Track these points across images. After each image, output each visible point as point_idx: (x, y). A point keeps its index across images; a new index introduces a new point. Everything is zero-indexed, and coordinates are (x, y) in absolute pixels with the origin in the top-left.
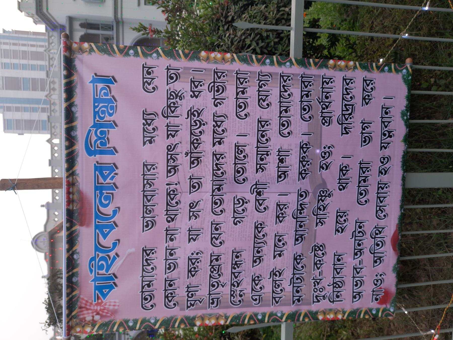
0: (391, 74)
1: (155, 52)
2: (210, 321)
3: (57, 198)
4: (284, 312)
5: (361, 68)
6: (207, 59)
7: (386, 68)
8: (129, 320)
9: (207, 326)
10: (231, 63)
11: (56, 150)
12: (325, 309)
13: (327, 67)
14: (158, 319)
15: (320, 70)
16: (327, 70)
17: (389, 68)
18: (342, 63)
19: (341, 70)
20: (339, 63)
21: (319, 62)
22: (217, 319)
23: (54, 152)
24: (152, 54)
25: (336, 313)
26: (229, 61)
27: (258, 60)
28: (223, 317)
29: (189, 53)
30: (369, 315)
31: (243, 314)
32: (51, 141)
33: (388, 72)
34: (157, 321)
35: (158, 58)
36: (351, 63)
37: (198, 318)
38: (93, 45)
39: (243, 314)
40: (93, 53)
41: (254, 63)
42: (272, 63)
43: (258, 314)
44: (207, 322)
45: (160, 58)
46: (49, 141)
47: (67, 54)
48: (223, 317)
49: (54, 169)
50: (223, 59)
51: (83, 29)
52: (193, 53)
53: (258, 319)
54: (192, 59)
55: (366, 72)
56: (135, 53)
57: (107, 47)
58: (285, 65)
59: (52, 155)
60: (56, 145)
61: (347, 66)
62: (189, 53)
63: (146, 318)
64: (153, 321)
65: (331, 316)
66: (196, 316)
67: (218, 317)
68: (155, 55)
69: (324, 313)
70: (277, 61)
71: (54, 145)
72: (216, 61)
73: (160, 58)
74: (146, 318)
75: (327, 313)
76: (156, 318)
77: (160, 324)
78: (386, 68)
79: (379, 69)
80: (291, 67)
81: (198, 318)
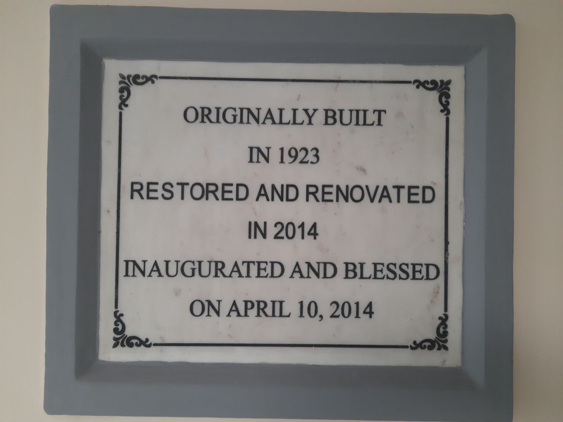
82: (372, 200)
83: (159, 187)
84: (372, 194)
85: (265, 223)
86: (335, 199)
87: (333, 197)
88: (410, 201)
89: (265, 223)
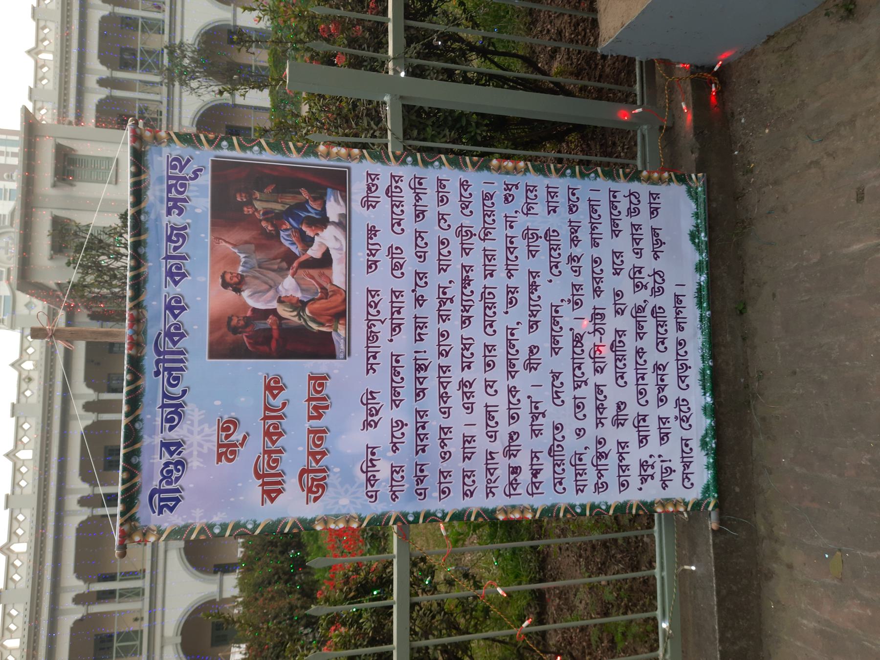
0: (575, 179)
1: (437, 160)
2: (337, 525)
3: (23, 483)
4: (446, 511)
5: (372, 158)
6: (328, 155)
7: (569, 171)
8: (215, 525)
9: (330, 529)
10: (360, 161)
11: (24, 444)
12: (326, 516)
13: (488, 168)
14: (258, 522)
15: (479, 173)
16: (489, 173)
17: (228, 143)
18: (509, 164)
19: (507, 173)
20: (505, 163)
21: (478, 162)
22: (348, 521)
23: (21, 433)
24: (433, 162)
25: (522, 512)
26: (357, 158)
27: (210, 142)
28: (154, 531)
29: (303, 147)
30: (483, 517)
31: (386, 514)
32: (14, 455)
33: (570, 176)
34: (256, 526)
35: (440, 168)
36: (666, 175)
37: (318, 521)
38: (529, 163)
39: (188, 526)
40: (364, 161)
41: (203, 145)
42: (573, 175)
43: (408, 514)
44: (332, 526)
45: (443, 167)
46: (11, 455)
47: (137, 145)
48: (355, 518)
49: (20, 423)
50: (349, 155)
51: (90, 414)
52: (308, 146)
53: (577, 513)
54: (306, 154)
55: (610, 181)
56: (572, 173)
57: (543, 166)
58: (432, 166)
59: (15, 484)
61: (515, 168)
62: (303, 147)
63: (240, 521)
64: (250, 526)
65: (517, 516)
66: (315, 518)
67: (349, 519)
68: (437, 163)
69: (325, 521)
70: (580, 172)
71: (19, 464)
72: (339, 158)
73: (443, 167)
74: (240, 521)
75: (509, 512)
76: (255, 522)
77: (450, 519)
78: (569, 171)
79: (213, 144)
80: (260, 153)
81: (318, 521)
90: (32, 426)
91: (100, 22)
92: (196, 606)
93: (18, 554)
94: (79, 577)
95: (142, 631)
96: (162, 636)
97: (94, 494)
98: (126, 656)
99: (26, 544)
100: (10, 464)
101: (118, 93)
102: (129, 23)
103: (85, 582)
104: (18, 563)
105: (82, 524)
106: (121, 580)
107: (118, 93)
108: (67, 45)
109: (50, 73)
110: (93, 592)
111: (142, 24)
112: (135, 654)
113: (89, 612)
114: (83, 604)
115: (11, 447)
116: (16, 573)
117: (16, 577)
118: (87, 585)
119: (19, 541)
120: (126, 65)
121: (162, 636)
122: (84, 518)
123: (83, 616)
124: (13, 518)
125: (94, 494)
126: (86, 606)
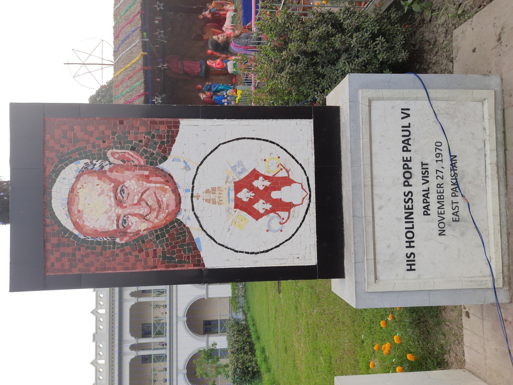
46: (94, 312)
51: (134, 298)
59: (97, 328)
60: (101, 365)
82: (444, 218)
83: (407, 205)
84: (442, 218)
85: (445, 235)
86: (443, 210)
87: (442, 210)
88: (444, 214)
89: (445, 235)
90: (104, 345)
91: (130, 309)
92: (193, 302)
93: (101, 314)
94: (132, 335)
95: (166, 323)
96: (177, 369)
97: (138, 291)
98: (159, 361)
99: (104, 310)
100: (93, 368)
101: (142, 299)
102: (146, 359)
103: (135, 338)
104: (101, 320)
105: (132, 360)
106: (154, 337)
107: (142, 299)
108: (112, 353)
109: (104, 321)
110: (140, 356)
111: (154, 358)
112: (163, 361)
113: (138, 355)
114: (135, 350)
115: (94, 307)
116: (101, 351)
117: (101, 327)
118: (136, 352)
119: (101, 307)
120: (146, 334)
121: (177, 369)
122: (133, 303)
123: (135, 303)
124: (97, 347)
125: (138, 291)
126: (137, 298)
